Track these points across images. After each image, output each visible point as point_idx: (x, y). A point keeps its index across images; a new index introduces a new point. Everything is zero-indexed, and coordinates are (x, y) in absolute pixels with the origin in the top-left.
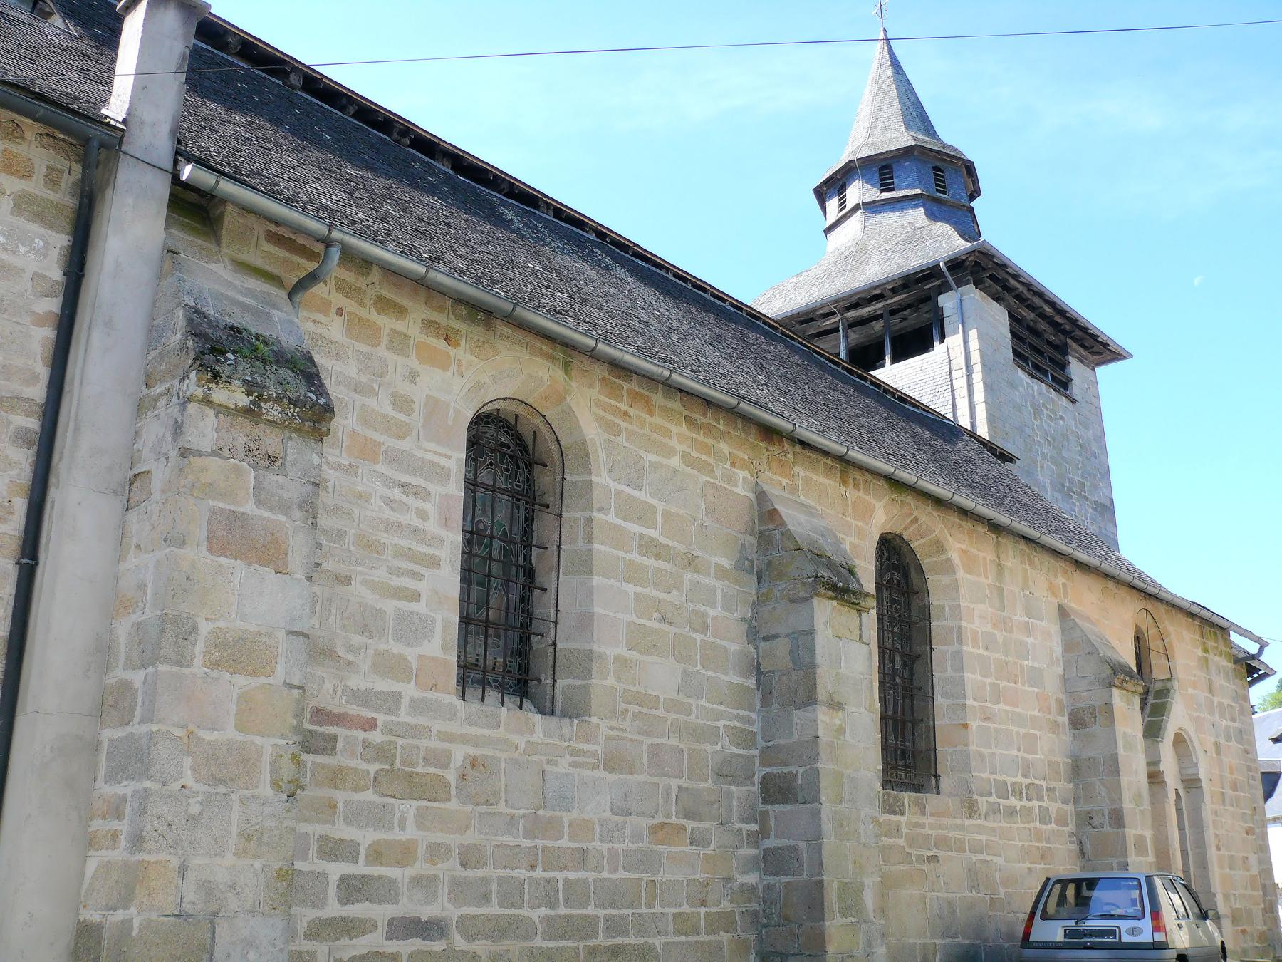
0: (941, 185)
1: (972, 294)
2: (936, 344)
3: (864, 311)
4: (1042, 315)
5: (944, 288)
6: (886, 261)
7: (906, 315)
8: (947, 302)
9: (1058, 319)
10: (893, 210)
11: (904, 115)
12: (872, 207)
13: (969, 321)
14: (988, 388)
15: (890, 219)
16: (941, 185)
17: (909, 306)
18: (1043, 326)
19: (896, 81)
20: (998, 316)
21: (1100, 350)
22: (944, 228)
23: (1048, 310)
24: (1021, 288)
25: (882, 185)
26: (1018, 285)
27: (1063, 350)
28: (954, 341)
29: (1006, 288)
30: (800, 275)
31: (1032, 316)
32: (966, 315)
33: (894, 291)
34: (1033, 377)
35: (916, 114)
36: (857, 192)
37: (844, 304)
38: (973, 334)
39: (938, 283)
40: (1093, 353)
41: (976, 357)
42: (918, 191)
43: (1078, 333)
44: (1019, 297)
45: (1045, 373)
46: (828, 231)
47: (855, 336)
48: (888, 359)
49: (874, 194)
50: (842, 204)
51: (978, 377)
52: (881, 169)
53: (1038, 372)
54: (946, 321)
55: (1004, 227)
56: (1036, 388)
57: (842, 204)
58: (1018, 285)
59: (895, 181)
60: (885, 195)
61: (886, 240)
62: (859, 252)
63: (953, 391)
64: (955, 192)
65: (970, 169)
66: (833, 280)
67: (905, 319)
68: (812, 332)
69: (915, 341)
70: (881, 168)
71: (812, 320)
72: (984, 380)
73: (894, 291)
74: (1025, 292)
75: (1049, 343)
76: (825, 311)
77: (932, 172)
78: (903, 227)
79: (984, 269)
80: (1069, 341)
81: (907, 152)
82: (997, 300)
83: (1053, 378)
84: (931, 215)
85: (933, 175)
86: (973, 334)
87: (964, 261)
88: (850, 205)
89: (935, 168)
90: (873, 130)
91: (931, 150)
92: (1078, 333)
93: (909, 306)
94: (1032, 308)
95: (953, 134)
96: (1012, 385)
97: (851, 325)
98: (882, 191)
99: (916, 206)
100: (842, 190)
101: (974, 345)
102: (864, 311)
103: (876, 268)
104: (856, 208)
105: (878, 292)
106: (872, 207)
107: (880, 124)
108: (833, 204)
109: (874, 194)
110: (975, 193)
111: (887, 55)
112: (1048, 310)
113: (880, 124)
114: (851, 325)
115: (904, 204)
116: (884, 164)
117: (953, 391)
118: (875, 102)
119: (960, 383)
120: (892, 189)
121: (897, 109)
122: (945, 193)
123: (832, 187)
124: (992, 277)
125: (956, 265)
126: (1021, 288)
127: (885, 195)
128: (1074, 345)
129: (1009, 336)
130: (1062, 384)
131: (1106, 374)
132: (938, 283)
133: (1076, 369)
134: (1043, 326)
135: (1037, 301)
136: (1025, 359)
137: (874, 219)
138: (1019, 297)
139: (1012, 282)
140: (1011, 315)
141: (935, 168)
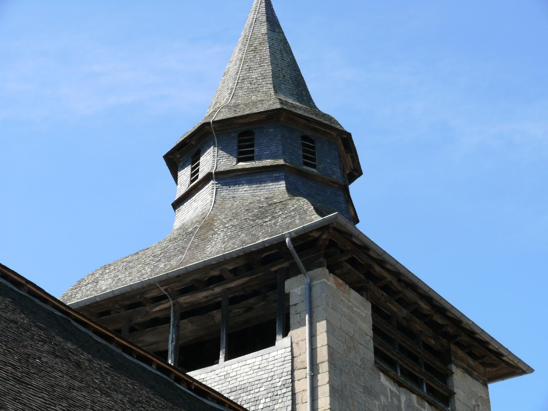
0: (310, 158)
1: (325, 281)
2: (279, 338)
3: (201, 296)
4: (417, 312)
5: (293, 271)
6: (231, 238)
7: (239, 302)
8: (295, 288)
9: (440, 320)
10: (250, 183)
11: (275, 76)
12: (224, 178)
13: (318, 311)
14: (334, 392)
15: (245, 192)
16: (310, 158)
17: (255, 293)
18: (418, 326)
19: (271, 40)
20: (359, 312)
21: (496, 363)
22: (304, 203)
23: (424, 306)
24: (389, 278)
25: (240, 153)
26: (385, 274)
27: (446, 358)
28: (300, 334)
29: (370, 276)
30: (137, 253)
31: (404, 312)
32: (315, 303)
33: (236, 273)
34: (400, 385)
35: (287, 73)
36: (210, 160)
37: (177, 286)
38: (322, 326)
39: (286, 265)
40: (484, 364)
41: (323, 354)
42: (281, 162)
43: (464, 338)
44: (386, 288)
45: (417, 381)
46: (177, 204)
47: (190, 327)
48: (222, 357)
49: (228, 163)
50: (195, 174)
51: (323, 378)
52: (240, 135)
53: (408, 380)
54: (292, 311)
55: (382, 213)
56: (403, 399)
57: (195, 174)
58: (385, 274)
59: (256, 149)
60: (242, 165)
61: (236, 216)
62: (206, 226)
63: (294, 394)
64: (327, 166)
65: (346, 140)
66: (169, 259)
67: (250, 309)
68: (139, 319)
69: (254, 337)
70: (237, 133)
71: (139, 304)
72: (331, 383)
73: (236, 273)
74: (395, 282)
75: (427, 347)
76: (153, 294)
77: (300, 141)
78: (259, 201)
79: (342, 251)
80: (453, 347)
81: (270, 117)
82: (359, 290)
83: (430, 390)
84: (293, 191)
85: (290, 139)
86: (322, 326)
87: (317, 239)
88: (201, 175)
89: (304, 138)
90: (218, 81)
91: (300, 116)
92: (464, 338)
93: (255, 293)
94: (403, 302)
95: (328, 97)
96: (369, 391)
97: (186, 314)
98: (239, 160)
99: (277, 180)
100: (195, 159)
101: (322, 339)
102: (201, 296)
103: (219, 245)
104: (208, 178)
105: (216, 273)
106: (224, 178)
107: (246, 85)
108: (185, 174)
109: (228, 163)
110: (355, 172)
111: (263, 10)
112: (424, 306)
113: (246, 85)
114: (186, 314)
115: (263, 176)
116: (244, 129)
117: (294, 394)
118: (244, 61)
119: (303, 386)
120: (251, 159)
121: (268, 69)
122: (314, 167)
123: (182, 155)
124: (352, 261)
125: (306, 241)
126: (389, 278)
127: (242, 165)
128: (460, 353)
129: (371, 333)
130: (443, 396)
131: (498, 390)
132: (286, 265)
133: (461, 382)
134: (418, 326)
135: (410, 295)
136: (391, 363)
137: (226, 192)
138: (386, 288)
139: (378, 269)
140: (376, 310)
141: (304, 138)
